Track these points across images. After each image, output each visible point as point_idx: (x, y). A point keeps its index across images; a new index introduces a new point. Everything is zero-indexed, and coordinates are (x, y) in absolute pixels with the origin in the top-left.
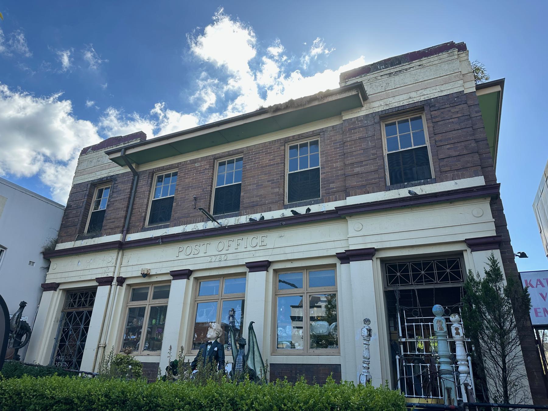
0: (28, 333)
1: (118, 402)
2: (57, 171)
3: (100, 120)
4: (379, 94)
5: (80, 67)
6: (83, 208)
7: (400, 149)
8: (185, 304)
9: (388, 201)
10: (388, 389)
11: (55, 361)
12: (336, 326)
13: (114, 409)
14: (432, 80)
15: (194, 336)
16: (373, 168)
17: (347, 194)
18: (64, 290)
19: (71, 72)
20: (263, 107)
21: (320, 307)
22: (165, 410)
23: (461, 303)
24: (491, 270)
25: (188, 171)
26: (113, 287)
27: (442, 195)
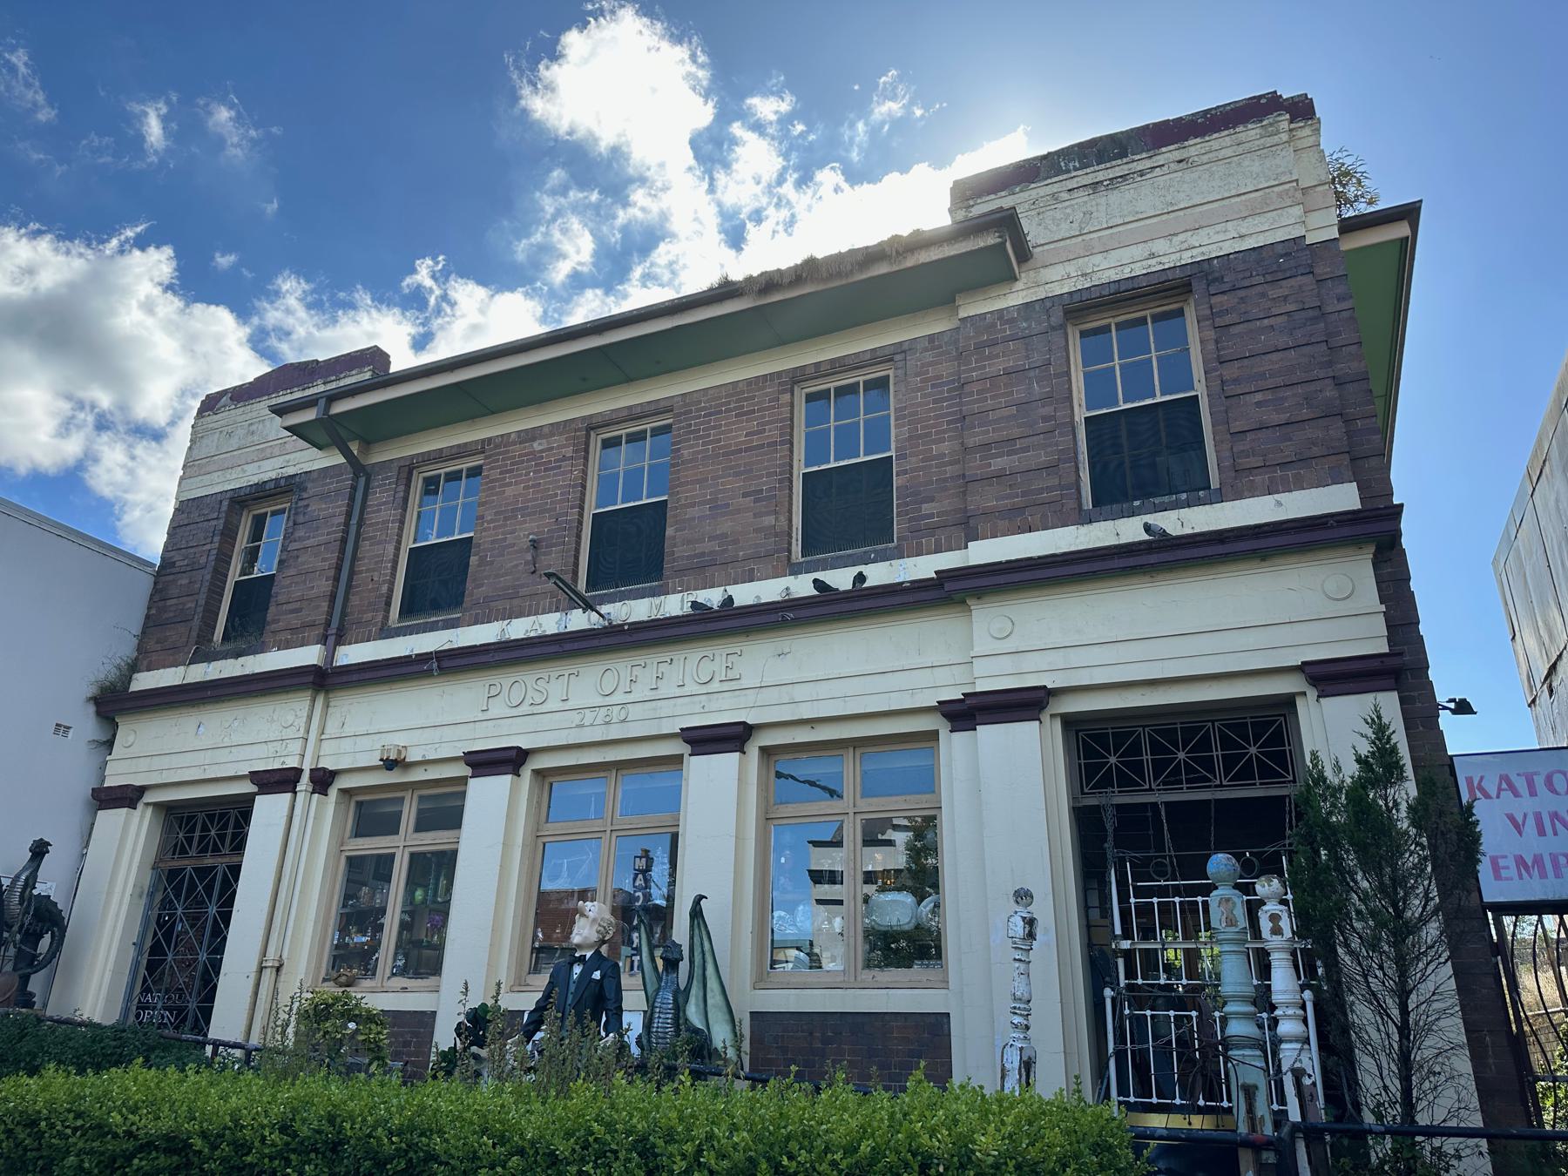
0: (56, 929)
1: (318, 1146)
2: (133, 458)
3: (254, 308)
4: (1062, 243)
5: (198, 151)
6: (210, 568)
7: (1121, 402)
8: (507, 845)
9: (1086, 554)
10: (1080, 1099)
11: (138, 1008)
12: (937, 906)
13: (307, 1167)
14: (1215, 205)
15: (535, 937)
16: (1044, 458)
17: (969, 530)
18: (157, 806)
19: (171, 166)
20: (729, 279)
21: (890, 843)
22: (453, 1169)
23: (1287, 842)
24: (1373, 753)
25: (512, 464)
26: (300, 797)
27: (1238, 537)
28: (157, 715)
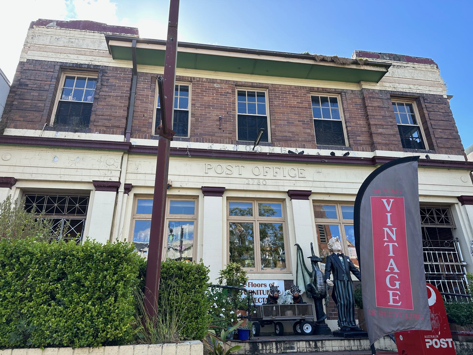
4: (387, 77)
26: (121, 194)
28: (25, 148)
